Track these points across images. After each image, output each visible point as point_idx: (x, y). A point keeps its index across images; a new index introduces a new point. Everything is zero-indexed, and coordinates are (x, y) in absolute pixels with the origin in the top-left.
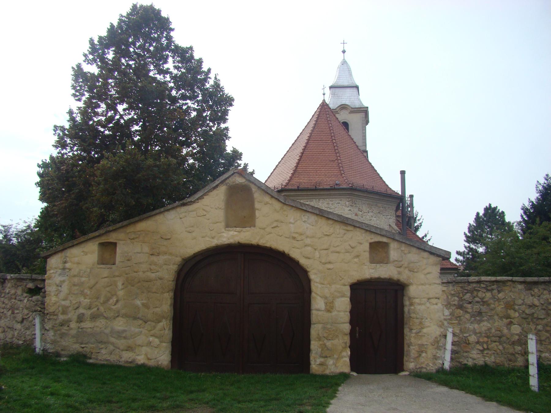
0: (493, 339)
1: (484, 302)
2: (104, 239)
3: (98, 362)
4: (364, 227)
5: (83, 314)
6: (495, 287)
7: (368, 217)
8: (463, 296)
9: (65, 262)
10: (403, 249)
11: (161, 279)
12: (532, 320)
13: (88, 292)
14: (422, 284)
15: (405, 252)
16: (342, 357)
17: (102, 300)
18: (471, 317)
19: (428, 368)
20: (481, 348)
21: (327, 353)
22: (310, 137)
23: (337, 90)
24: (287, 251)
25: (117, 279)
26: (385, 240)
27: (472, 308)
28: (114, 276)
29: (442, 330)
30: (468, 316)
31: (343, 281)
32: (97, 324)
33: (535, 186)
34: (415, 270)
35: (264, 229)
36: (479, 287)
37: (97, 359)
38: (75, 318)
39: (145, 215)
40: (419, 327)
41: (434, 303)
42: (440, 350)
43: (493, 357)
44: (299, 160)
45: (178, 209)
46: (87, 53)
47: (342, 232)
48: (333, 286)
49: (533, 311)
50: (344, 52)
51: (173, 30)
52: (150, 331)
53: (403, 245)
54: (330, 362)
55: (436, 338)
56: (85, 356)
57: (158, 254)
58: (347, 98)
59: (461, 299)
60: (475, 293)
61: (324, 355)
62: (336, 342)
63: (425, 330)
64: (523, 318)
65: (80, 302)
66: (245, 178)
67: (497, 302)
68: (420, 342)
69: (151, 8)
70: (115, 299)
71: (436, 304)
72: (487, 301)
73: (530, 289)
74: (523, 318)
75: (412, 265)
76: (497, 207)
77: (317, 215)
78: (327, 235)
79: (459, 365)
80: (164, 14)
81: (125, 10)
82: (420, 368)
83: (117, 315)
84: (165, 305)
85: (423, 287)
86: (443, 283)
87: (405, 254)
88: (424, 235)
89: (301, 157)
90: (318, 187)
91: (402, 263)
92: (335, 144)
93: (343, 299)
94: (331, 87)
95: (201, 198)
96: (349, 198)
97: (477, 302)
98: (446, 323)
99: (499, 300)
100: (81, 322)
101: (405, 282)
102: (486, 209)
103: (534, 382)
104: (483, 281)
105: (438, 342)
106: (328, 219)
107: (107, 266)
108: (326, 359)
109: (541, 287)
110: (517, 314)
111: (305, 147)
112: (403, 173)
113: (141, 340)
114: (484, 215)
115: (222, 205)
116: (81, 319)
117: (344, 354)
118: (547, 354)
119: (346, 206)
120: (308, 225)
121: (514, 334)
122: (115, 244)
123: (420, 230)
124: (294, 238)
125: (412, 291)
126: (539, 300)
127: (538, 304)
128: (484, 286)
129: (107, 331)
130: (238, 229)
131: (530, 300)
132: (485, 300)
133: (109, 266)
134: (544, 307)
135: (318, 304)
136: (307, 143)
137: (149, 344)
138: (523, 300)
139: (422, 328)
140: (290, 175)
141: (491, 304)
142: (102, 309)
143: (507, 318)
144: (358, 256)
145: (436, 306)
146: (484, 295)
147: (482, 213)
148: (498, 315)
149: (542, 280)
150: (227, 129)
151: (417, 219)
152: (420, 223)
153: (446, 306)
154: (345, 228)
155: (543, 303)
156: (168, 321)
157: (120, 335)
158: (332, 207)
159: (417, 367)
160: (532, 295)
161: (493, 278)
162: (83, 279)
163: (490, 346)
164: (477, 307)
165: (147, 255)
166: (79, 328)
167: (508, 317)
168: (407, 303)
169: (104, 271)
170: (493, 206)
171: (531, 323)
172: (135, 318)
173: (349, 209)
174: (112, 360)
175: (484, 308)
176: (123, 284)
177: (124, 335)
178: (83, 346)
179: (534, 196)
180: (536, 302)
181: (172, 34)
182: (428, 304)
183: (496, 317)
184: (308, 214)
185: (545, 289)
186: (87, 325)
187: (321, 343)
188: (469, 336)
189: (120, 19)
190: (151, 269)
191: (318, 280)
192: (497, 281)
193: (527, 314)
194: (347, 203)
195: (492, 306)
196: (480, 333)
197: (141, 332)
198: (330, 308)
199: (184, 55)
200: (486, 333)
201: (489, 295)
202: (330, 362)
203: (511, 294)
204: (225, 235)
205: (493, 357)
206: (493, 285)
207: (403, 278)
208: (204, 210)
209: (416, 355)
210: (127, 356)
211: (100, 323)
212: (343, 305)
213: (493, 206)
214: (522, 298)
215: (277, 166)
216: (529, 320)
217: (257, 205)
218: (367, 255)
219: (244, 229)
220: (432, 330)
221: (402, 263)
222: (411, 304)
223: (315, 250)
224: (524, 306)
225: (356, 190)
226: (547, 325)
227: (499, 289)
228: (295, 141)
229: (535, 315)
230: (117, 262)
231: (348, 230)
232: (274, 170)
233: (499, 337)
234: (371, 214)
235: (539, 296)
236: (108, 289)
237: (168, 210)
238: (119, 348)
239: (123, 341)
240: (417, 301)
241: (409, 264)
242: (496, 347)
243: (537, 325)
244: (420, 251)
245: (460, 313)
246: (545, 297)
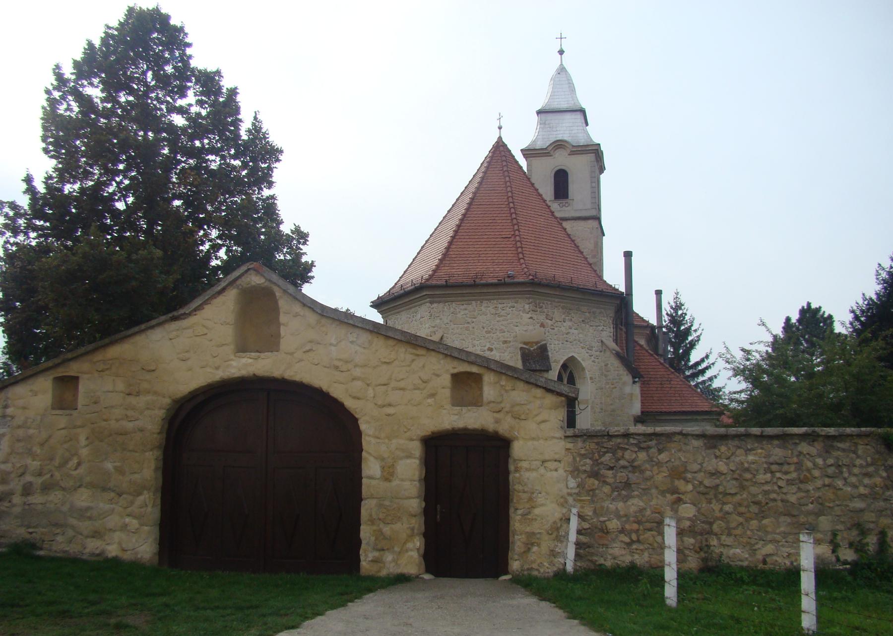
0: (648, 525)
1: (634, 468)
2: (61, 372)
3: (52, 554)
4: (442, 350)
5: (31, 483)
6: (653, 443)
7: (563, 329)
8: (600, 458)
9: (6, 407)
10: (503, 383)
11: (142, 430)
12: (716, 496)
13: (37, 450)
14: (533, 439)
15: (507, 388)
16: (407, 551)
17: (57, 462)
18: (613, 491)
19: (542, 570)
20: (627, 540)
21: (384, 544)
22: (472, 199)
23: (550, 117)
24: (325, 388)
25: (79, 430)
26: (474, 369)
27: (615, 476)
28: (75, 427)
29: (564, 511)
30: (607, 489)
31: (408, 434)
32: (50, 498)
33: (874, 272)
34: (523, 417)
35: (292, 354)
36: (627, 444)
37: (50, 550)
38: (19, 489)
39: (118, 336)
40: (528, 506)
41: (552, 468)
42: (562, 542)
43: (646, 554)
44: (453, 237)
45: (167, 326)
46: (51, 88)
47: (409, 357)
48: (394, 441)
49: (717, 481)
50: (561, 52)
51: (189, 45)
52: (125, 508)
53: (504, 377)
54: (389, 557)
55: (555, 522)
56: (34, 546)
57: (138, 394)
58: (566, 129)
59: (596, 462)
60: (620, 453)
61: (379, 547)
62: (397, 526)
63: (537, 511)
64: (699, 493)
65: (26, 466)
66: (264, 277)
67: (656, 468)
68: (528, 529)
69: (157, 11)
70: (75, 460)
71: (556, 470)
72: (639, 466)
73: (715, 447)
74: (699, 493)
75: (517, 408)
76: (820, 307)
77: (371, 332)
78: (385, 363)
79: (593, 567)
80: (174, 21)
81: (116, 17)
82: (528, 569)
83: (78, 484)
84: (147, 468)
85: (535, 443)
86: (566, 437)
87: (507, 391)
88: (704, 355)
89: (456, 232)
90: (478, 281)
91: (502, 405)
92: (512, 210)
93: (408, 461)
94: (539, 112)
95: (199, 308)
96: (529, 298)
97: (624, 467)
98: (570, 500)
99: (659, 464)
100: (28, 494)
101: (507, 435)
102: (803, 312)
103: (670, 592)
104: (632, 434)
105: (558, 529)
106: (388, 337)
107: (64, 411)
108: (382, 552)
109: (731, 443)
110: (690, 487)
111: (464, 215)
112: (628, 255)
113: (113, 521)
114: (799, 321)
115: (231, 318)
116: (27, 490)
117: (410, 545)
118: (738, 550)
119: (524, 311)
120: (358, 348)
121: (684, 518)
122: (76, 379)
123: (697, 347)
124: (337, 368)
125: (518, 449)
126: (727, 464)
127: (725, 472)
128: (635, 442)
129: (65, 508)
130: (253, 354)
131: (712, 464)
132: (636, 464)
133: (68, 412)
134: (736, 476)
135: (371, 468)
136: (467, 210)
137: (124, 527)
138: (701, 464)
139: (533, 507)
140: (436, 262)
141: (646, 470)
142: (57, 475)
143: (672, 494)
144: (433, 395)
145: (554, 473)
146: (634, 456)
147: (795, 317)
148: (657, 488)
149: (734, 433)
150: (272, 197)
151: (693, 328)
152: (698, 337)
153: (572, 472)
154: (414, 351)
155: (733, 468)
156: (151, 494)
157: (83, 514)
158: (503, 313)
159: (526, 567)
160: (716, 457)
161: (649, 430)
162: (31, 431)
163: (641, 537)
164: (622, 475)
165: (122, 394)
166: (25, 504)
167: (674, 491)
168: (512, 468)
169: (61, 420)
170: (813, 306)
171: (714, 501)
172: (104, 489)
173: (529, 315)
174: (71, 551)
175: (634, 477)
176: (87, 438)
177: (89, 514)
178: (31, 530)
179: (872, 289)
180: (723, 467)
181: (189, 51)
182: (542, 470)
183: (653, 491)
184: (357, 331)
185: (739, 447)
186: (37, 499)
187: (375, 528)
188: (609, 520)
189: (105, 33)
190: (127, 416)
191: (371, 432)
192: (655, 434)
193: (707, 487)
194: (527, 306)
195: (648, 473)
196: (626, 516)
197: (113, 509)
198: (388, 474)
199: (209, 82)
200: (636, 517)
201: (642, 455)
202: (389, 557)
203: (680, 454)
204: (234, 363)
205: (646, 554)
206: (651, 440)
207: (504, 428)
208: (204, 326)
209: (522, 550)
210: (93, 546)
211: (55, 497)
212: (410, 470)
213: (813, 306)
214: (699, 461)
215: (422, 247)
216: (711, 495)
217: (283, 318)
218: (447, 393)
219: (262, 355)
220: (548, 510)
221: (502, 405)
222: (517, 470)
223: (368, 385)
224: (702, 474)
225: (540, 285)
226: (740, 505)
227: (661, 447)
228: (453, 206)
229: (721, 489)
230: (80, 406)
231: (418, 355)
232: (418, 253)
233: (657, 523)
234: (570, 324)
235: (728, 458)
236: (66, 446)
237: (152, 327)
238: (81, 534)
239: (87, 523)
240: (524, 464)
241: (513, 406)
242: (651, 539)
243: (724, 503)
244: (530, 386)
245: (594, 485)
246: (737, 459)
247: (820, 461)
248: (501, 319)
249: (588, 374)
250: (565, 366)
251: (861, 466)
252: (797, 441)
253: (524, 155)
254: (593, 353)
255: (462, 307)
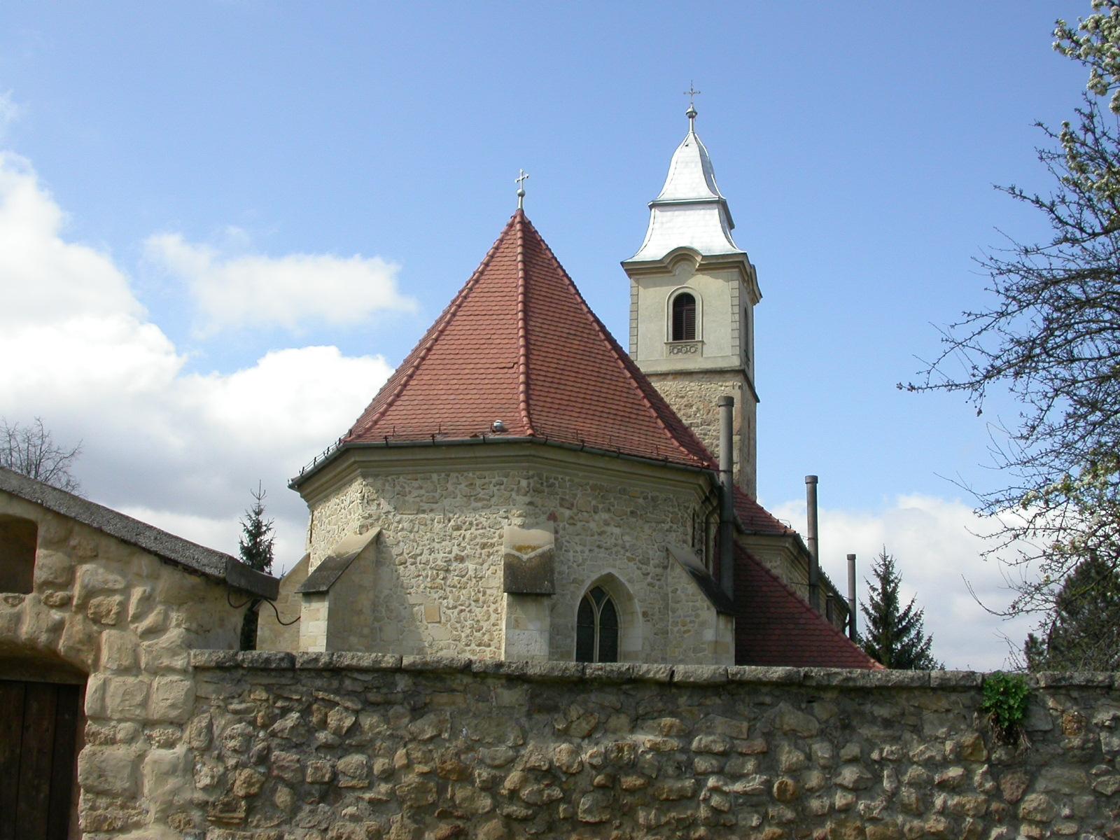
7: (592, 525)
36: (337, 692)
73: (554, 709)
109: (594, 698)
173: (527, 499)
194: (524, 483)
234: (605, 516)
247: (822, 751)
248: (480, 504)
249: (638, 607)
250: (597, 591)
251: (930, 764)
252: (768, 700)
253: (626, 270)
254: (650, 569)
255: (416, 484)
